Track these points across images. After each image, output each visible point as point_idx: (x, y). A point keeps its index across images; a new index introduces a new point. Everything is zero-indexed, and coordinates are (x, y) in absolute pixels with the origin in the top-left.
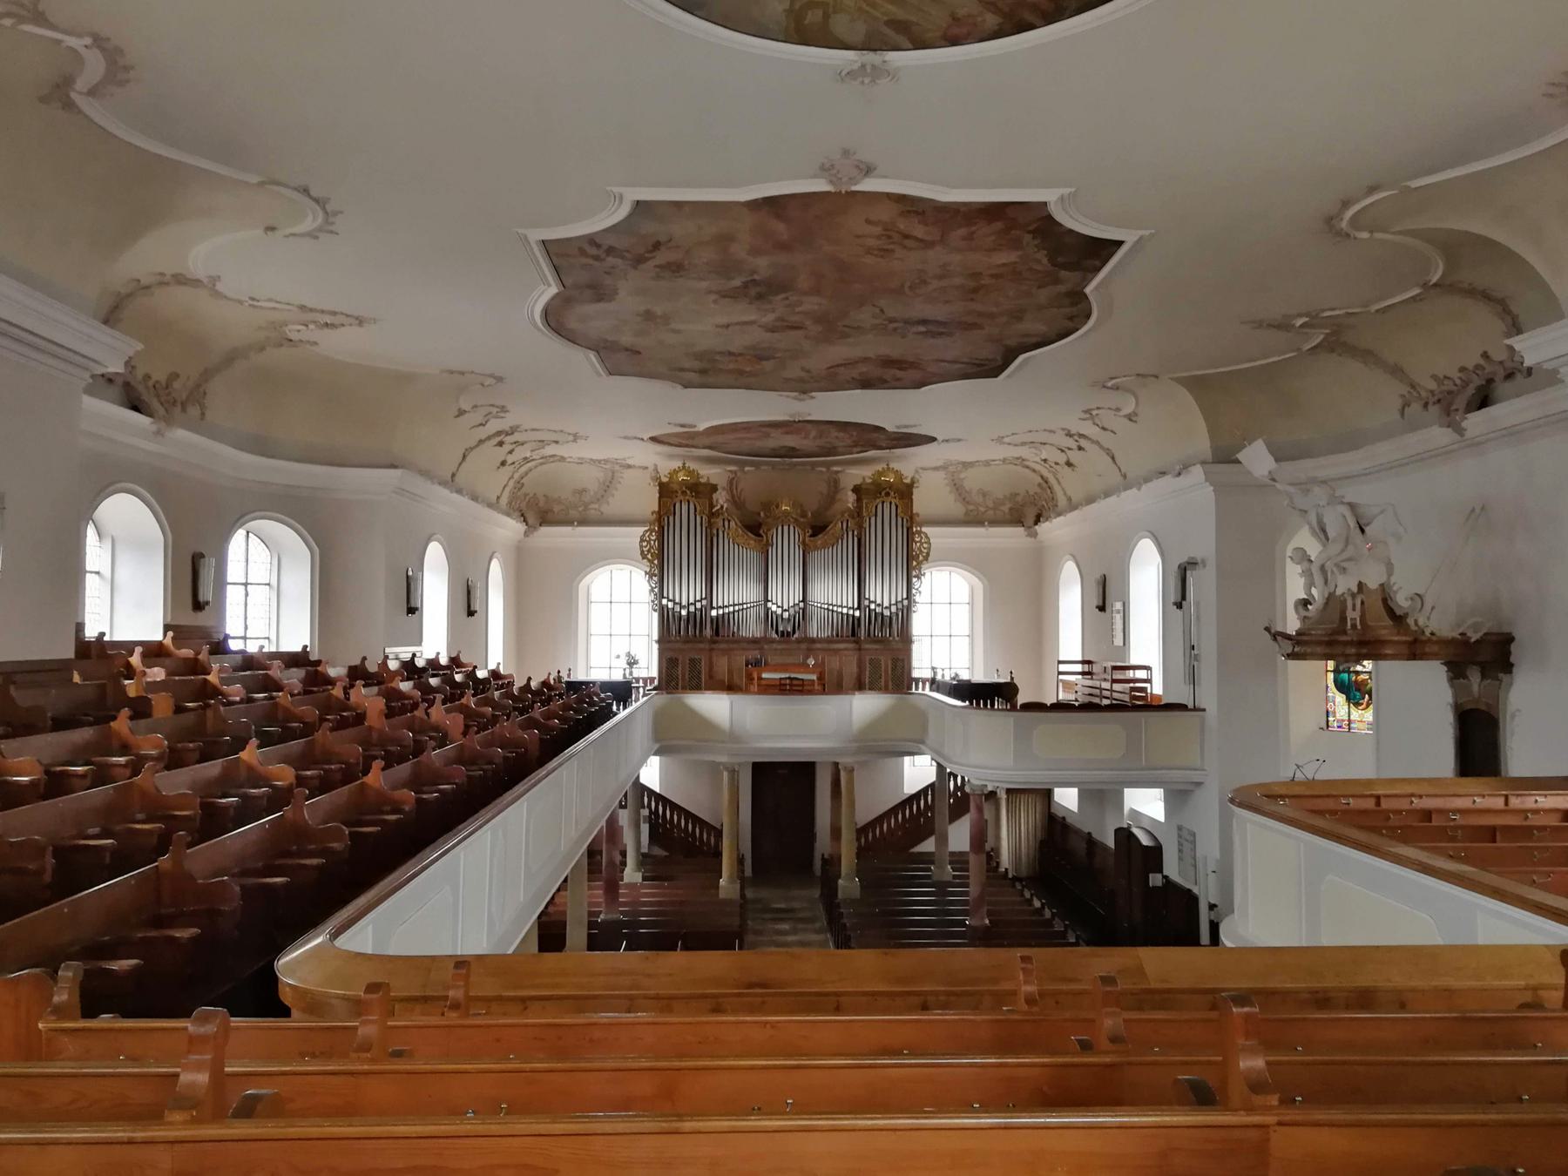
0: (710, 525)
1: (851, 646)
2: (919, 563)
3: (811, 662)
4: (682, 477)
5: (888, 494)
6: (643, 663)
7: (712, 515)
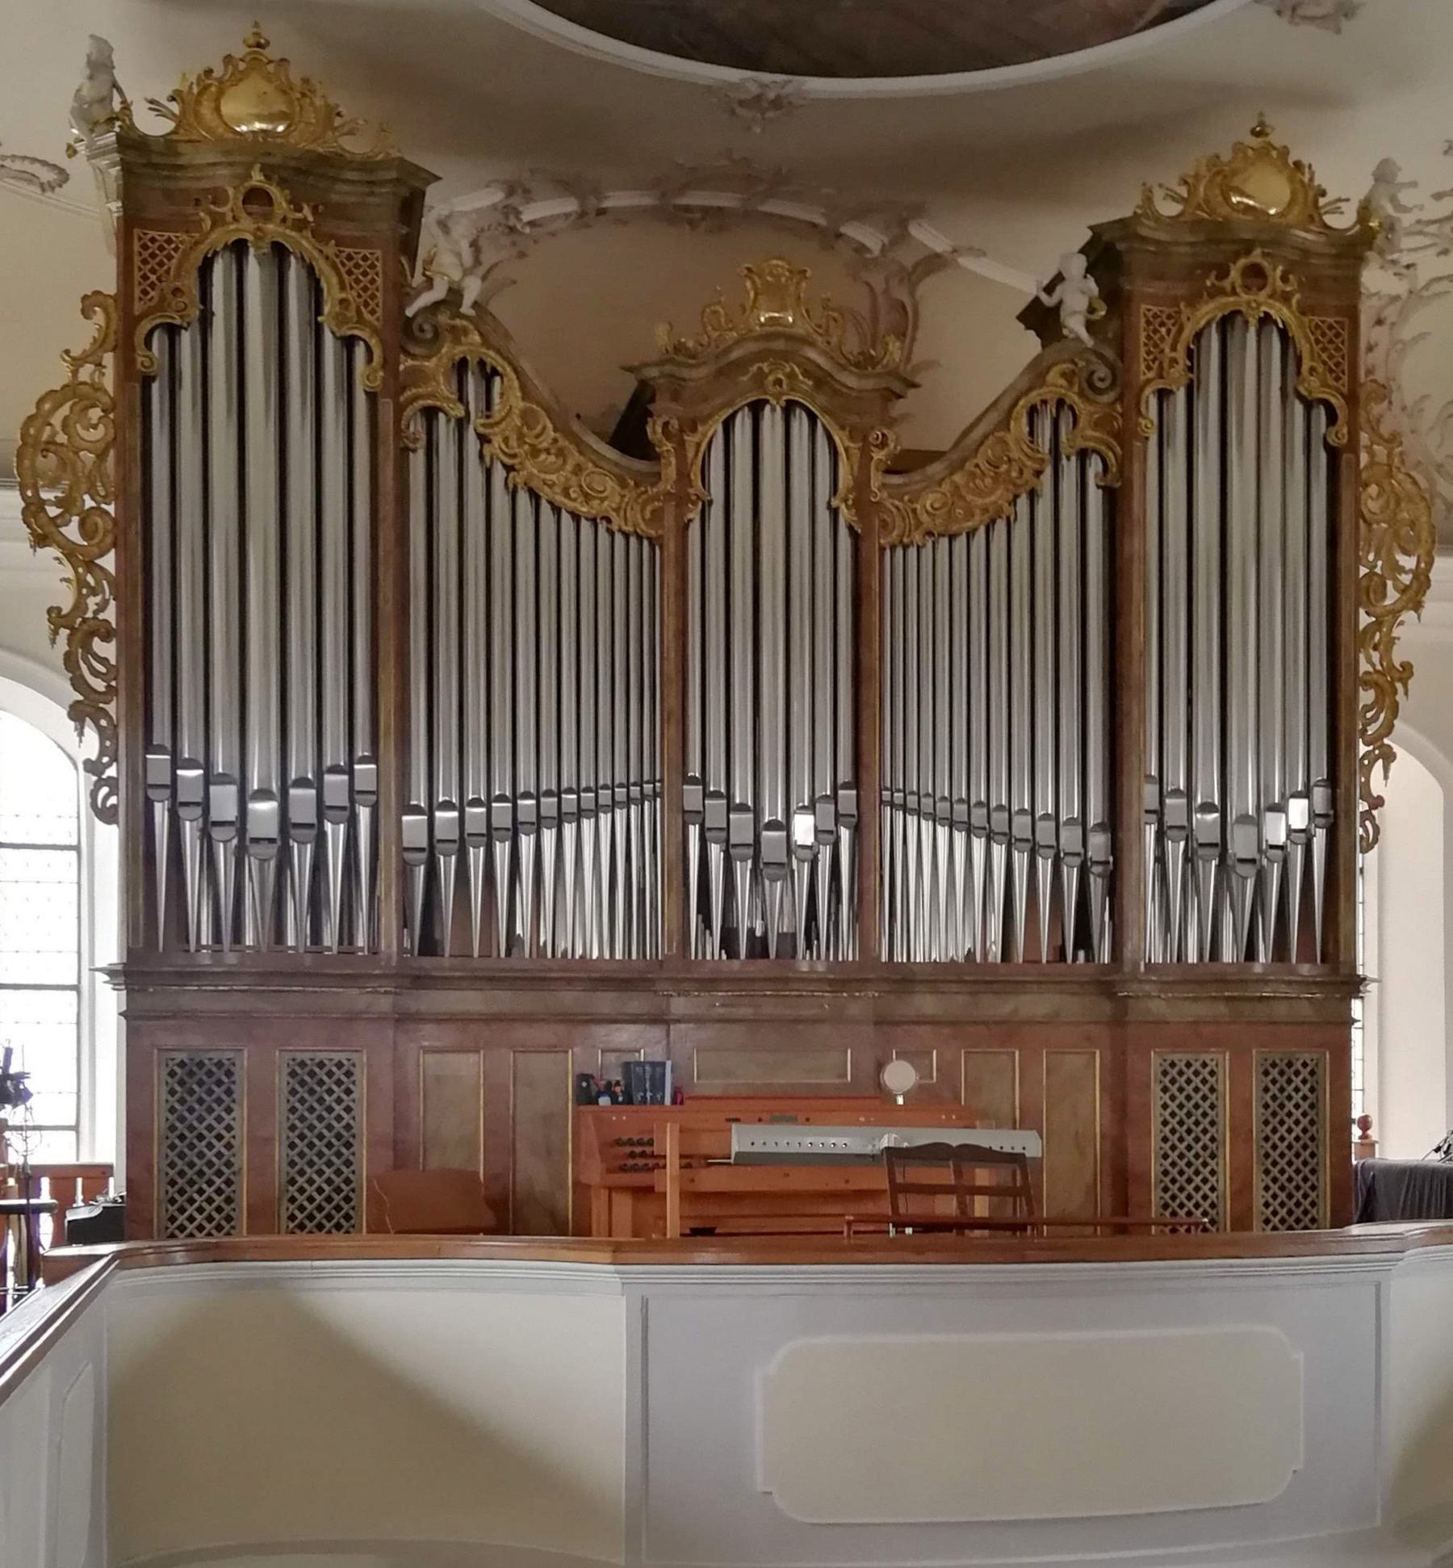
0: (397, 384)
1: (1072, 1006)
2: (1386, 620)
3: (900, 1077)
4: (246, 115)
5: (1255, 275)
6: (50, 1094)
7: (405, 334)
